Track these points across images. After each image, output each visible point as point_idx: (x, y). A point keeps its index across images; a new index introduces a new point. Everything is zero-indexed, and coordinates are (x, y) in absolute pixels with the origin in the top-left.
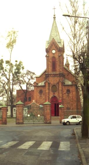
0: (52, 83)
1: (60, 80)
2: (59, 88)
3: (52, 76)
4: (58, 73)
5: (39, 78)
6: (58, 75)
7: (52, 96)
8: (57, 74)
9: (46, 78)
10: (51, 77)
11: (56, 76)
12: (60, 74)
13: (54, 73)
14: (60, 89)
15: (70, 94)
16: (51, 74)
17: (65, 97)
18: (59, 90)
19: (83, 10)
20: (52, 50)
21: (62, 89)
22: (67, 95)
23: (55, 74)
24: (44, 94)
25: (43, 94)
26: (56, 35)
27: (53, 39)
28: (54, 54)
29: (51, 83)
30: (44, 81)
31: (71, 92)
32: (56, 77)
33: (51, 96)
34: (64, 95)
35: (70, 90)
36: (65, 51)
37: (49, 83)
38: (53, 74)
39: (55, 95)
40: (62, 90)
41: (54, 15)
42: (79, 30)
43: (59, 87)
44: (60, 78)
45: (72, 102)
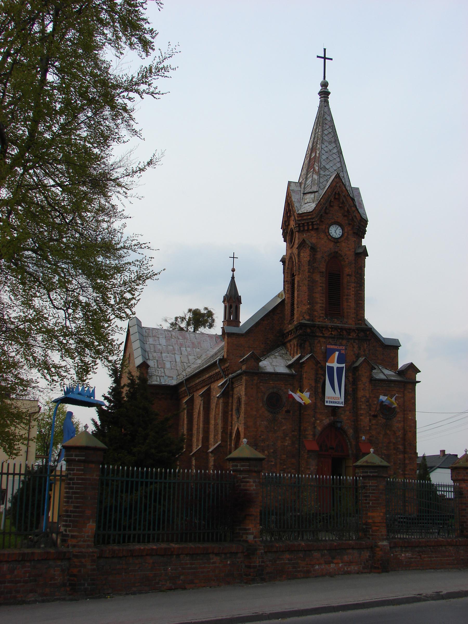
6: (353, 335)
8: (349, 331)
10: (322, 340)
11: (343, 339)
16: (326, 328)
23: (342, 329)
25: (284, 409)
28: (336, 241)
41: (325, 85)
44: (359, 348)
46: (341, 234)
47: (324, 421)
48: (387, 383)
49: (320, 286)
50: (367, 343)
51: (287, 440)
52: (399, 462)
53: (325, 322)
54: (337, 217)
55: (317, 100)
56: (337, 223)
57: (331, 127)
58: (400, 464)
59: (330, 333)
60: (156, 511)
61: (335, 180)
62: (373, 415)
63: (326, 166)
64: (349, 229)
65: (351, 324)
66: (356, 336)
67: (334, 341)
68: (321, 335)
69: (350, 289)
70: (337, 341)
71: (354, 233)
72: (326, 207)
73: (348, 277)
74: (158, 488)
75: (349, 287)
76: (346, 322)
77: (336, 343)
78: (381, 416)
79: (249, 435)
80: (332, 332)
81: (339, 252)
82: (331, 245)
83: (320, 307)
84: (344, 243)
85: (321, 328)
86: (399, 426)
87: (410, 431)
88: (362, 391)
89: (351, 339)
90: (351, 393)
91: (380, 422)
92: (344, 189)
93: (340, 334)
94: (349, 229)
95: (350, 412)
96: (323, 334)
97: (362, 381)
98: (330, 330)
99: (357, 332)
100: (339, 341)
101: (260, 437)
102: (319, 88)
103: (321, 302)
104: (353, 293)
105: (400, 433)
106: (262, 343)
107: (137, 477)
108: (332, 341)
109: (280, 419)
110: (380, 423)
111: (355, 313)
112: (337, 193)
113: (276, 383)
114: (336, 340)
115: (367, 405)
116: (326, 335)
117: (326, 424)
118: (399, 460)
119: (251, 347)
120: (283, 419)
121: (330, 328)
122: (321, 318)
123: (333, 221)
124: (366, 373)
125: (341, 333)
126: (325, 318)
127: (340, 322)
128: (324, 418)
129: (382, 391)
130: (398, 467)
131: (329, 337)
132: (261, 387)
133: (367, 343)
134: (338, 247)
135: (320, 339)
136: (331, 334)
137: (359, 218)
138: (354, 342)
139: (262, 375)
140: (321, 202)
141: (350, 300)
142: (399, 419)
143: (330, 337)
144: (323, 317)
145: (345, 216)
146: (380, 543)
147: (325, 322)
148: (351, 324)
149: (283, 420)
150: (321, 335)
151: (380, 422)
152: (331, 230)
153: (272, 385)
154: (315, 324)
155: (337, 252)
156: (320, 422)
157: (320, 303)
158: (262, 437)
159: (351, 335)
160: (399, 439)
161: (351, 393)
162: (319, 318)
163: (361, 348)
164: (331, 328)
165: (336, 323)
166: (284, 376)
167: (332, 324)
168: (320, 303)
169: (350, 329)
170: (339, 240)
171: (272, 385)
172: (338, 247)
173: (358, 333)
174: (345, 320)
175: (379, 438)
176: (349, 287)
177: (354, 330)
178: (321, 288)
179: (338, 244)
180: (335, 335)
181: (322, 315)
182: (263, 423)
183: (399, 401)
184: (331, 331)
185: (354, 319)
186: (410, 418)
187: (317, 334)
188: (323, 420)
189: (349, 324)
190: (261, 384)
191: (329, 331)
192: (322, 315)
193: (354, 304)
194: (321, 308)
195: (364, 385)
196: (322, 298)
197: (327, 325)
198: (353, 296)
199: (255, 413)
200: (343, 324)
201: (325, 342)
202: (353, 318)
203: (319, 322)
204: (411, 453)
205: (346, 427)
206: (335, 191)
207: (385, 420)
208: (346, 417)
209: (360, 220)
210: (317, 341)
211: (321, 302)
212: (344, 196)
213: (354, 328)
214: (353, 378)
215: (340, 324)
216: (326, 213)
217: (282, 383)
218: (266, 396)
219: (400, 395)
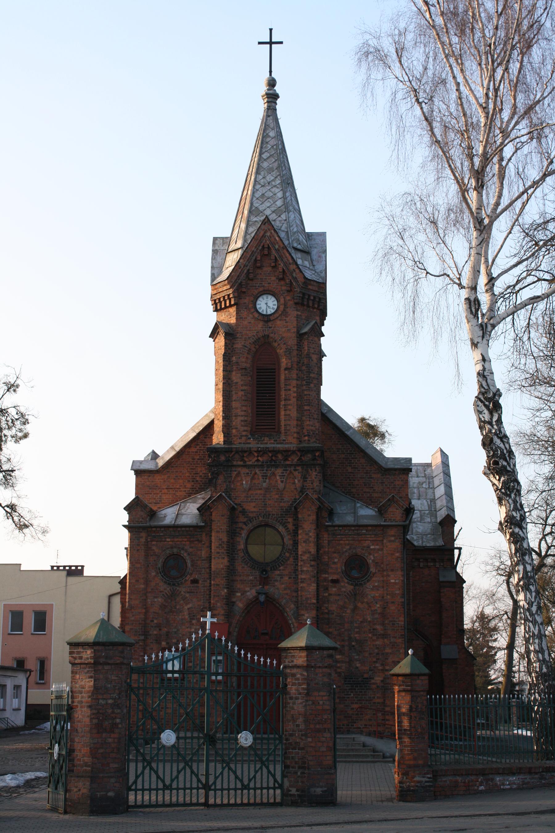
0: (251, 507)
1: (302, 490)
2: (296, 544)
3: (251, 461)
4: (291, 443)
5: (158, 479)
6: (295, 459)
7: (251, 594)
8: (287, 453)
9: (215, 475)
10: (244, 471)
11: (277, 466)
12: (303, 451)
13: (270, 444)
14: (301, 549)
15: (369, 585)
16: (250, 452)
17: (333, 607)
18: (296, 559)
19: (483, 363)
20: (257, 298)
21: (319, 547)
22: (350, 588)
23: (275, 452)
24: (195, 581)
25: (189, 578)
26: (279, 203)
27: (267, 221)
28: (267, 319)
29: (244, 512)
30: (191, 494)
31: (373, 570)
32: (279, 471)
33: (244, 593)
34: (326, 589)
35: (370, 560)
36: (124, 537)
37: (233, 509)
38: (262, 452)
39: (270, 589)
40: (317, 558)
41: (272, 83)
42: (529, 166)
43: (301, 537)
44: (305, 478)
45: (384, 636)
46: (276, 307)
47: (248, 594)
48: (353, 528)
49: (242, 390)
50: (316, 470)
51: (193, 624)
52: (376, 651)
53: (250, 443)
54: (269, 283)
55: (261, 106)
56: (267, 292)
57: (275, 147)
58: (378, 654)
59: (256, 459)
60: (349, 755)
61: (263, 227)
62: (332, 580)
63: (259, 207)
64: (288, 298)
65: (291, 443)
66: (298, 460)
67: (263, 470)
68: (241, 463)
69: (290, 390)
70: (266, 470)
71: (296, 304)
72: (249, 270)
73: (287, 372)
74: (448, 724)
75: (288, 387)
76: (284, 440)
77: (266, 473)
78: (346, 581)
79: (133, 619)
80: (259, 458)
81: (272, 335)
82: (261, 325)
83: (242, 421)
84: (280, 320)
85: (243, 453)
86: (377, 595)
87: (393, 603)
88: (304, 545)
89: (290, 466)
90: (291, 548)
91: (343, 589)
92: (277, 239)
93: (272, 459)
94: (288, 298)
95: (289, 578)
96: (245, 462)
97: (303, 528)
98: (256, 455)
99: (299, 454)
100: (271, 470)
101: (152, 621)
102: (264, 89)
103: (243, 413)
104: (295, 395)
105: (378, 606)
106: (189, 481)
107: (436, 704)
108: (260, 470)
109: (182, 593)
110: (345, 592)
111: (297, 425)
112: (267, 246)
113: (176, 540)
114: (265, 469)
115: (311, 566)
116: (248, 463)
117: (251, 597)
118: (377, 648)
119: (172, 488)
120: (188, 592)
121: (255, 451)
122: (244, 438)
123: (261, 289)
124: (309, 515)
125: (274, 458)
126: (250, 436)
127: (273, 442)
128: (248, 589)
129: (347, 542)
130: (375, 660)
131: (254, 466)
132: (154, 548)
133: (316, 470)
134: (270, 328)
135: (239, 469)
136: (258, 460)
137: (301, 280)
138: (295, 470)
139: (154, 529)
140: (240, 263)
141: (289, 407)
142: (376, 584)
143: (256, 465)
144: (246, 436)
145: (280, 280)
146: (55, 758)
147: (250, 443)
148: (291, 443)
149: (187, 595)
150: (241, 463)
151: (343, 589)
152: (260, 304)
153: (171, 543)
154: (232, 448)
155: (268, 336)
156: (242, 595)
157: (242, 416)
158: (155, 621)
159: (290, 459)
160: (377, 616)
161: (291, 548)
162: (240, 438)
163: (307, 478)
164: (258, 451)
165: (266, 443)
166: (188, 529)
167: (259, 446)
168: (242, 416)
169: (287, 451)
170: (272, 318)
171: (171, 543)
172: (270, 328)
173: (301, 456)
174: (283, 437)
175: (344, 614)
176: (288, 387)
177: (294, 452)
178: (243, 393)
179: (270, 324)
180: (263, 462)
181: (244, 433)
182: (156, 600)
183: (375, 555)
184: (258, 456)
185: (295, 435)
186: (392, 581)
187: (235, 463)
188: (246, 592)
189: (287, 443)
190: (154, 543)
191: (255, 456)
192: (244, 433)
193: (295, 412)
194: (243, 423)
195: (307, 534)
196: (244, 408)
197: (250, 448)
198: (295, 400)
199: (143, 586)
200: (278, 443)
201: (248, 473)
202: (295, 433)
203: (240, 443)
204: (395, 637)
205: (284, 601)
206: (262, 244)
207: (352, 587)
208: (283, 586)
209: (305, 283)
210: (236, 473)
211: (243, 413)
212: (277, 251)
213: (295, 449)
214: (294, 525)
215: (274, 443)
216: (248, 278)
217: (186, 540)
218: (161, 560)
219: (377, 547)
